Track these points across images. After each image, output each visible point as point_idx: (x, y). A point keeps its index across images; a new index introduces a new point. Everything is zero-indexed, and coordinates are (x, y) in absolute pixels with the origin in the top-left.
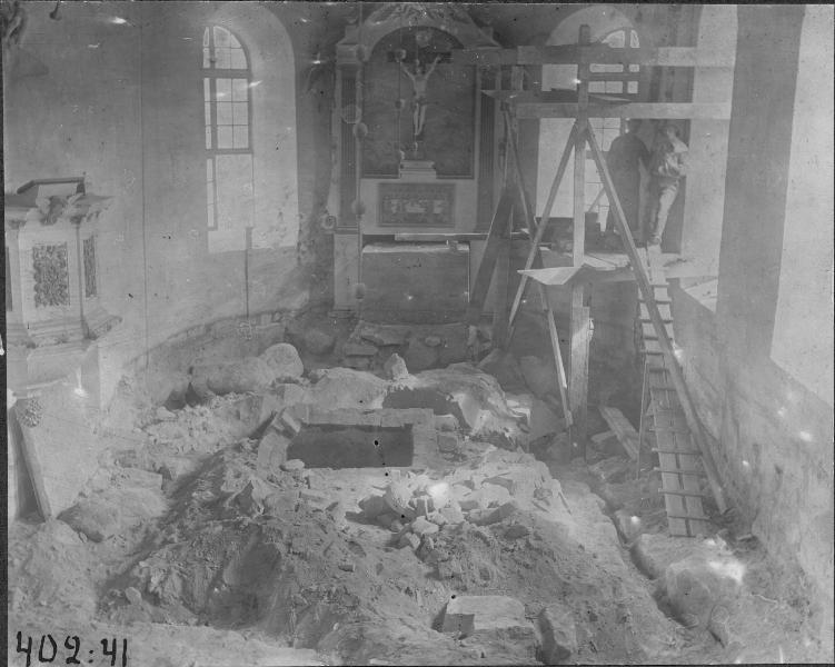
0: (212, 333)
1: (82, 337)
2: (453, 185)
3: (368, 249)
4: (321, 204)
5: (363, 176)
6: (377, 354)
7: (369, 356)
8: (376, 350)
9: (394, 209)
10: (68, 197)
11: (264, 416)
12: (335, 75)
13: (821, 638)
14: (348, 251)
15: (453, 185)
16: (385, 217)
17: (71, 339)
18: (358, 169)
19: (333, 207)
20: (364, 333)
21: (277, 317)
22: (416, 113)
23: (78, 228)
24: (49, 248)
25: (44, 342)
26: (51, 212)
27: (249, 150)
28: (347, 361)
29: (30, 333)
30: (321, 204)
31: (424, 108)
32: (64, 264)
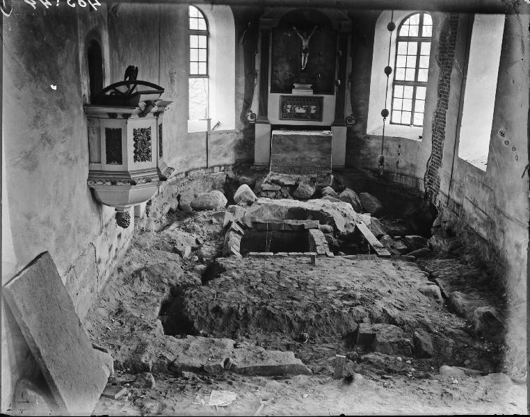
0: (188, 177)
1: (158, 179)
2: (322, 97)
3: (274, 132)
4: (248, 104)
5: (271, 92)
6: (280, 190)
7: (275, 191)
8: (280, 188)
9: (289, 111)
10: (155, 101)
11: (225, 222)
12: (258, 35)
13: (92, 295)
14: (261, 130)
15: (322, 97)
16: (284, 115)
17: (153, 180)
18: (269, 88)
19: (255, 108)
20: (275, 178)
21: (223, 168)
22: (303, 58)
23: (157, 119)
24: (142, 129)
25: (139, 182)
26: (146, 109)
27: (207, 76)
28: (263, 194)
29: (132, 177)
30: (248, 104)
31: (308, 55)
32: (149, 139)
